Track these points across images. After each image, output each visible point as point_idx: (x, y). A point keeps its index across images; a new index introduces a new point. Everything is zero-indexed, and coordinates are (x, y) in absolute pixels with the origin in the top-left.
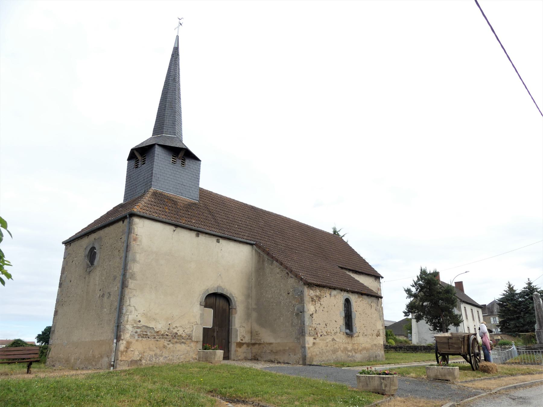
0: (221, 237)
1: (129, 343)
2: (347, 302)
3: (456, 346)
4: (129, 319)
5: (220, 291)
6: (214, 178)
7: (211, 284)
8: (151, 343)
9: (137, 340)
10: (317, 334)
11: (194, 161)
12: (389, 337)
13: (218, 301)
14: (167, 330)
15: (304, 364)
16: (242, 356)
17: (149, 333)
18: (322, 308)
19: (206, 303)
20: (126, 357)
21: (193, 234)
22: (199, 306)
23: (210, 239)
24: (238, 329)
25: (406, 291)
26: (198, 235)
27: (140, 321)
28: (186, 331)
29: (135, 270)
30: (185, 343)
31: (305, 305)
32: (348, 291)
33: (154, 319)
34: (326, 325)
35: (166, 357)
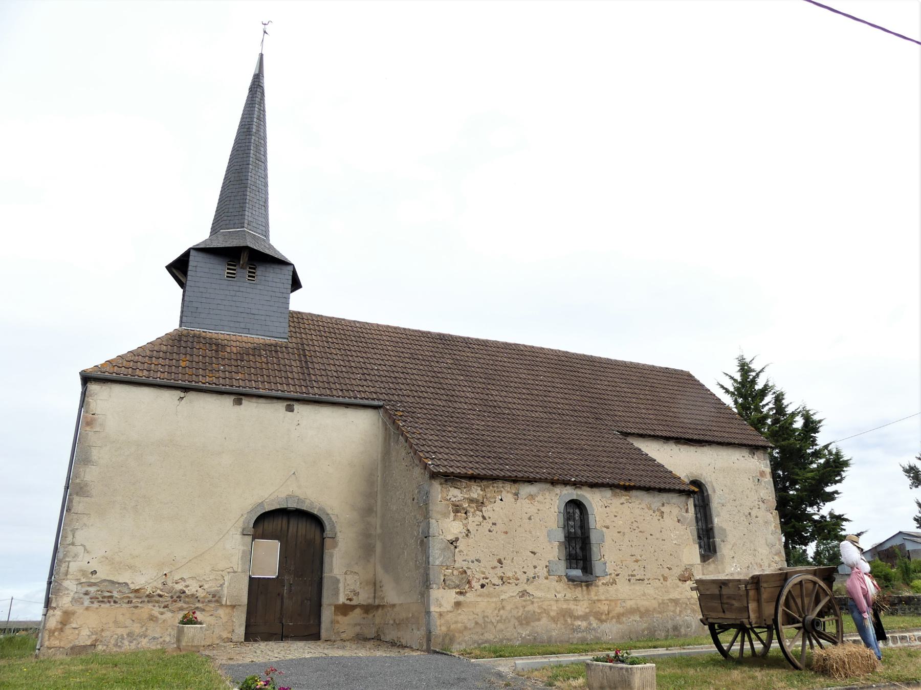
0: (297, 400)
1: (67, 616)
2: (576, 505)
3: (736, 604)
4: (70, 570)
5: (292, 505)
6: (320, 296)
7: (273, 492)
8: (122, 612)
9: (87, 609)
10: (469, 582)
11: (276, 266)
12: (912, 575)
13: (292, 526)
14: (160, 586)
15: (428, 650)
16: (350, 632)
17: (115, 594)
18: (487, 525)
19: (255, 532)
20: (60, 640)
21: (228, 401)
22: (238, 537)
23: (269, 405)
24: (338, 577)
25: (906, 471)
26: (238, 402)
27: (94, 573)
28: (206, 586)
29: (88, 478)
30: (204, 610)
31: (433, 521)
32: (576, 485)
33: (130, 567)
34: (500, 562)
35: (154, 638)
